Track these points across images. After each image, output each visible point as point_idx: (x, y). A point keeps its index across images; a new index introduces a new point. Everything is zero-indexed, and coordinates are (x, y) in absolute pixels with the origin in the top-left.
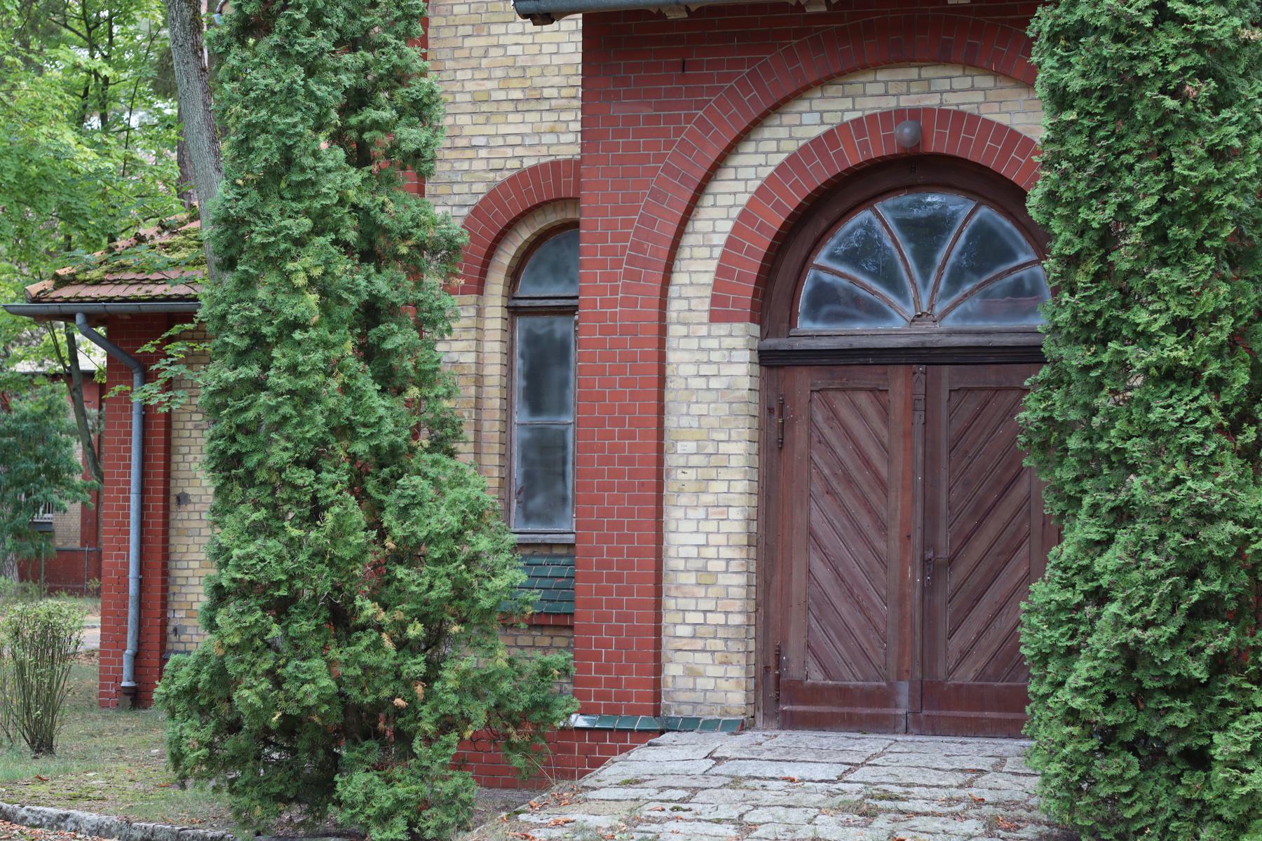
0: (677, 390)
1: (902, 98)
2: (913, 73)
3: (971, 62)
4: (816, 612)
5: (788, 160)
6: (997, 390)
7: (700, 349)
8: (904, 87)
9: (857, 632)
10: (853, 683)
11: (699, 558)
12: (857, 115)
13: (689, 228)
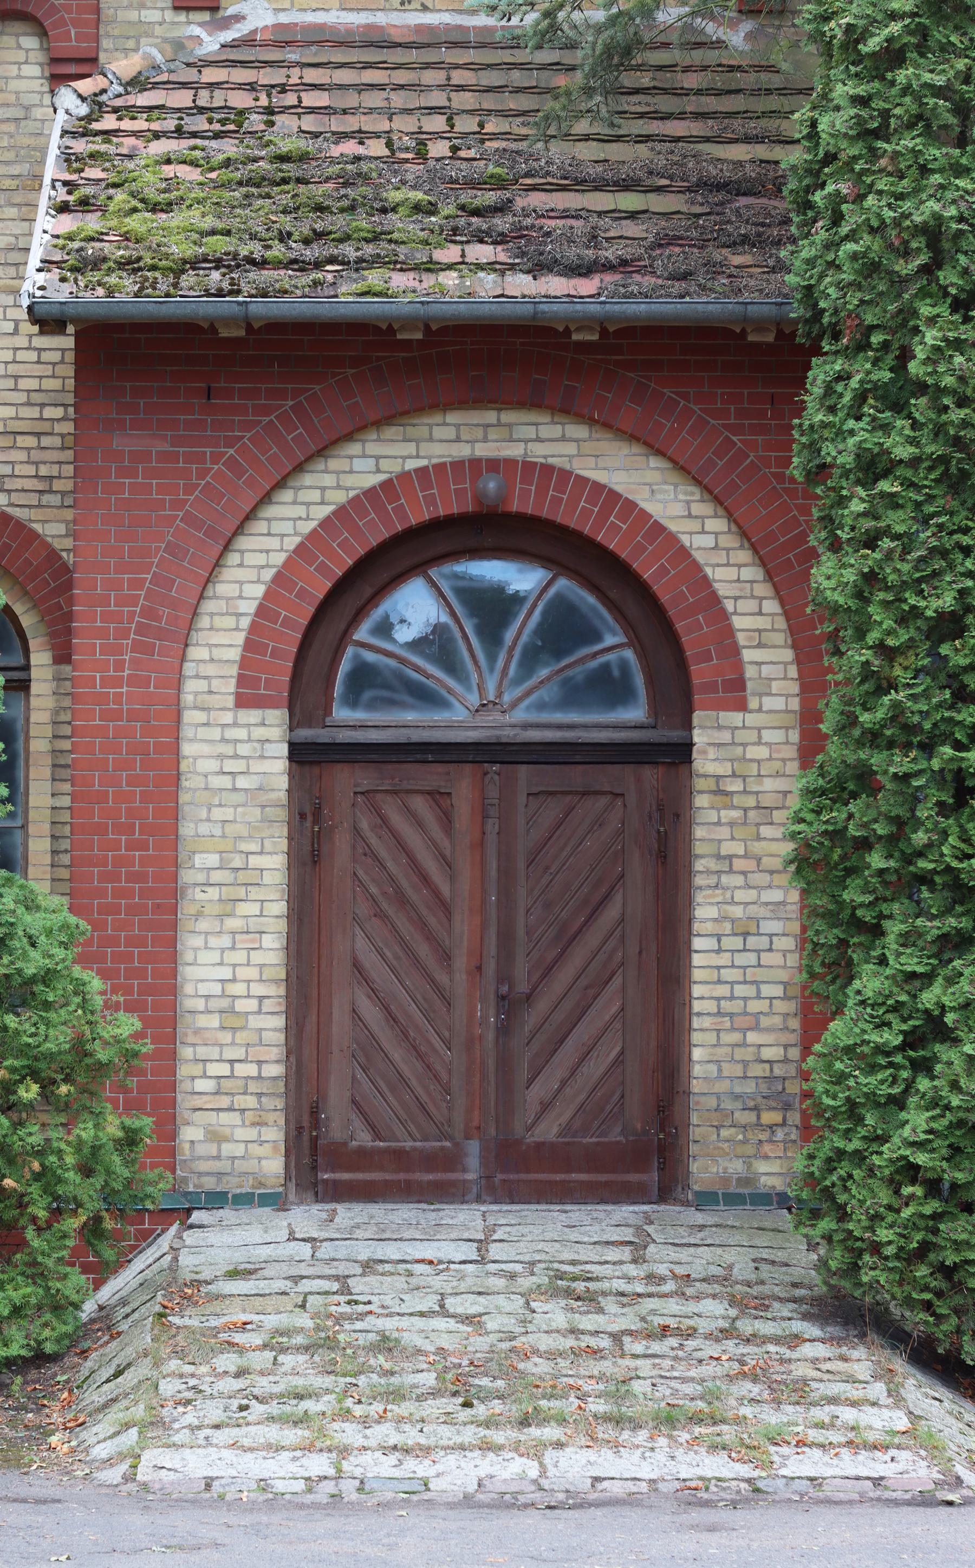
0: (195, 790)
1: (477, 445)
2: (491, 416)
3: (565, 408)
4: (362, 1060)
5: (334, 513)
6: (584, 794)
7: (223, 740)
8: (479, 433)
9: (414, 1082)
10: (409, 1144)
11: (223, 995)
12: (423, 463)
13: (209, 592)
